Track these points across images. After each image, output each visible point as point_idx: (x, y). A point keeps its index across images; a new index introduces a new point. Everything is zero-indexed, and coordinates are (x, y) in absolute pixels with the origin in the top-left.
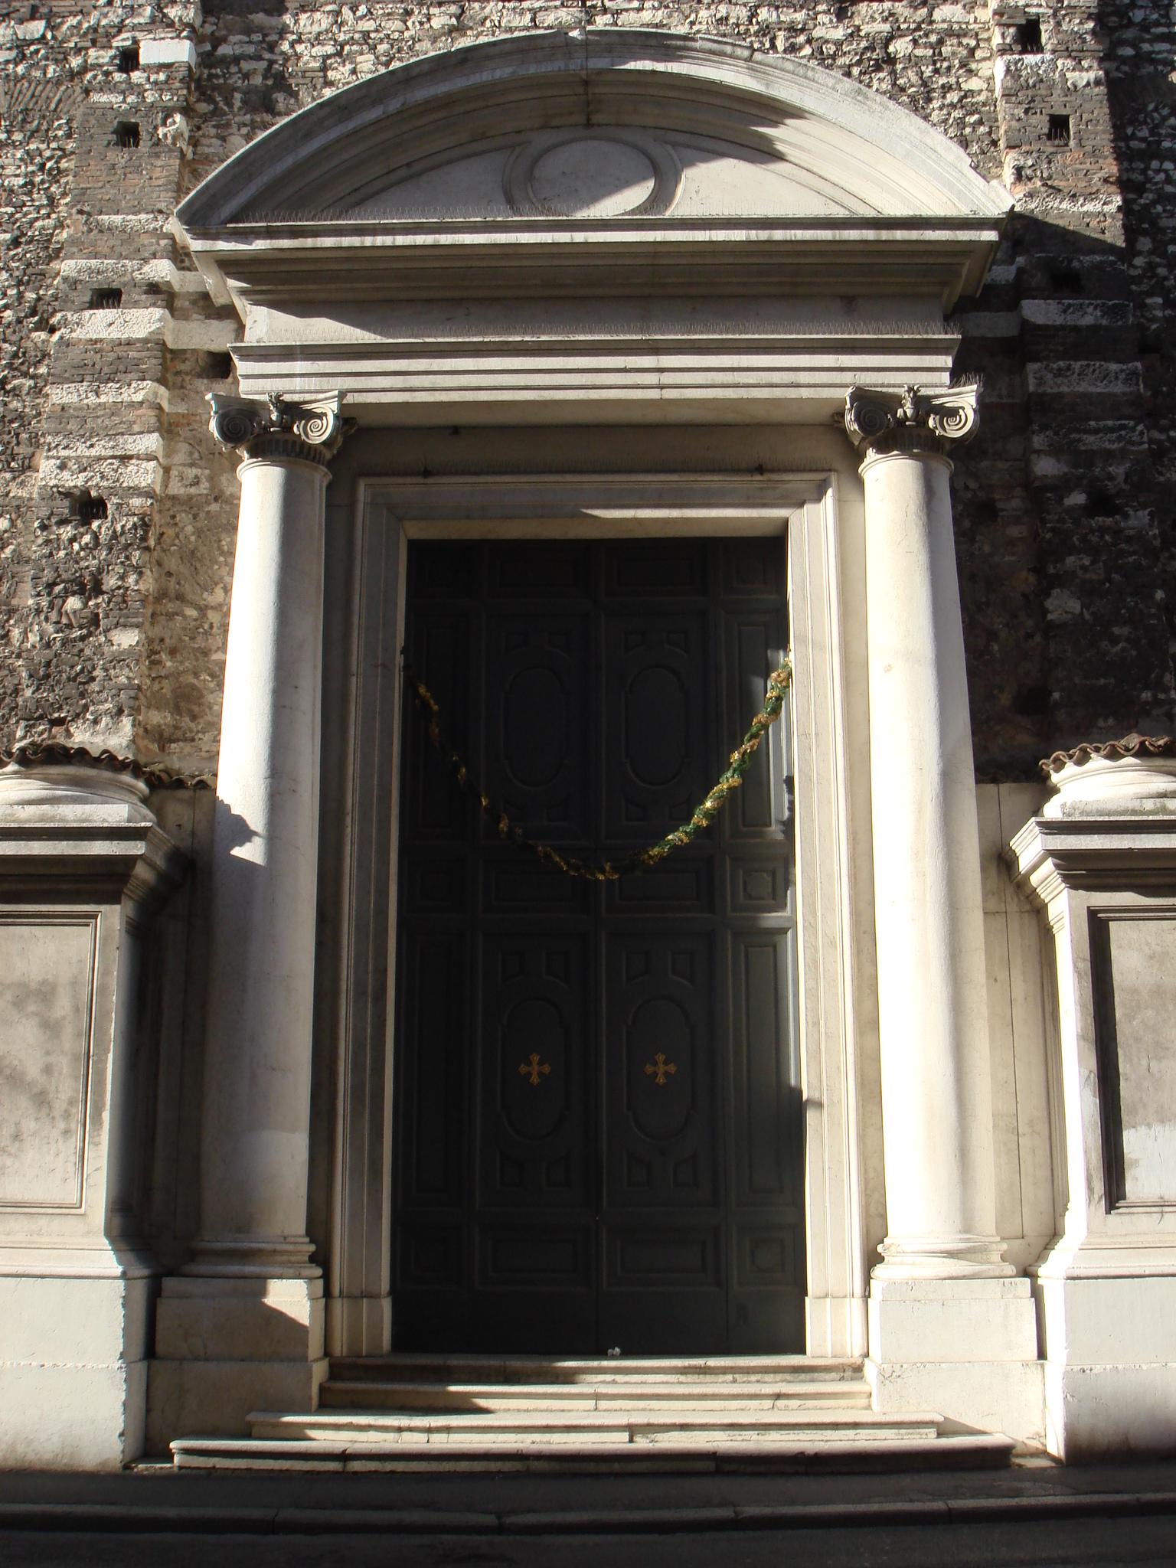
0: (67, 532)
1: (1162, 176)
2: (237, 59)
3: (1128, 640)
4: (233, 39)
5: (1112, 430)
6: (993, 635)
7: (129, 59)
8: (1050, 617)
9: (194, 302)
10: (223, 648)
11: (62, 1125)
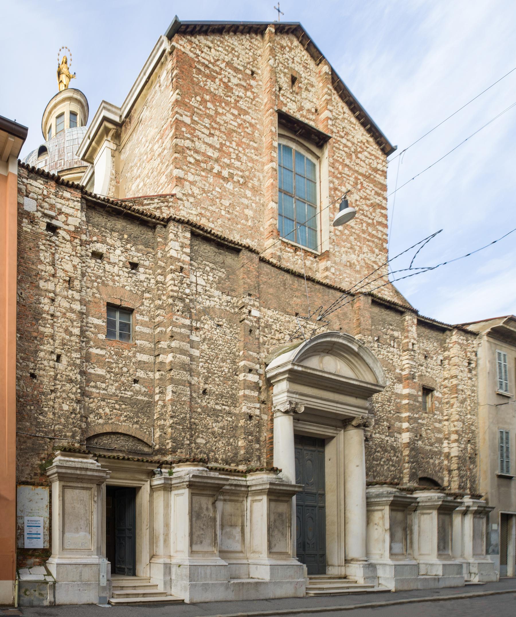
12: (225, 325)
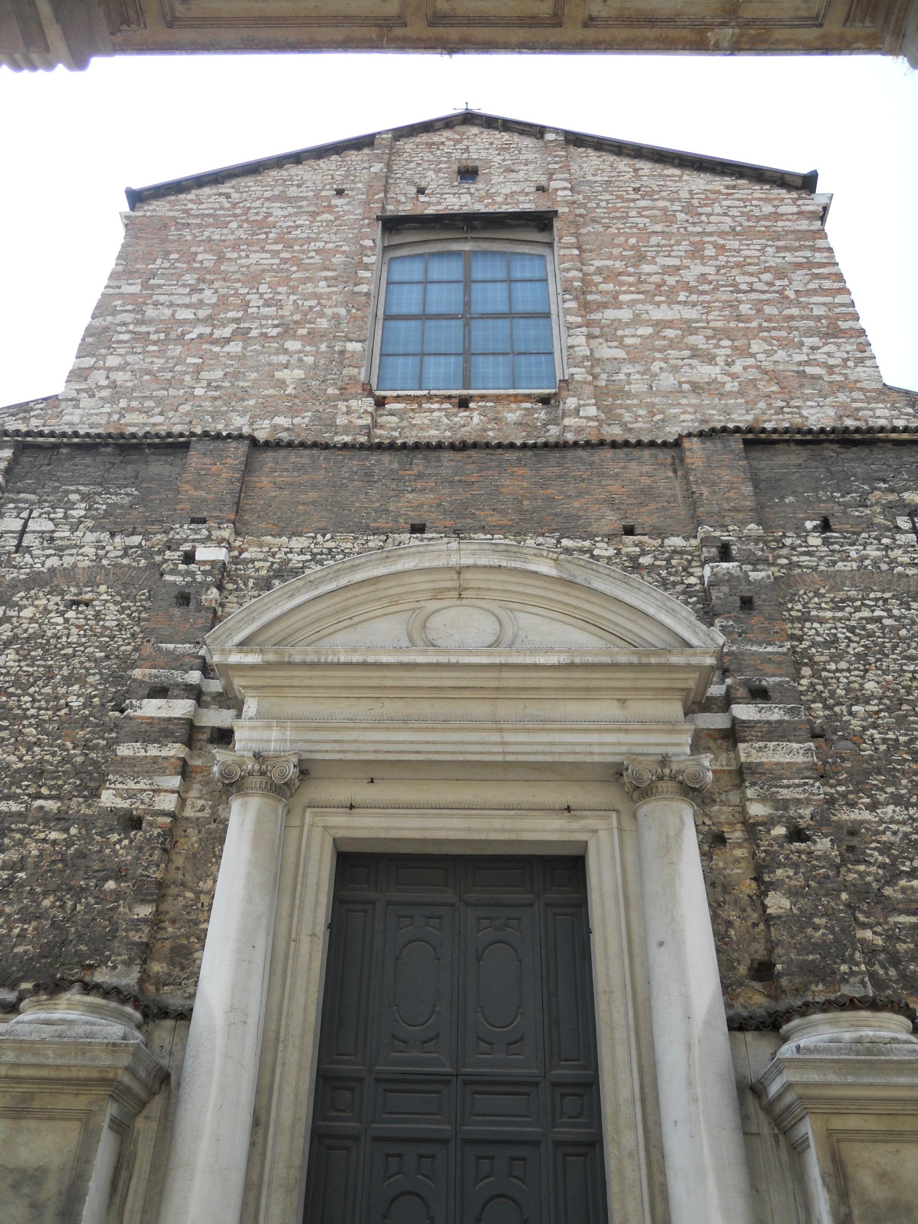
3: (826, 927)
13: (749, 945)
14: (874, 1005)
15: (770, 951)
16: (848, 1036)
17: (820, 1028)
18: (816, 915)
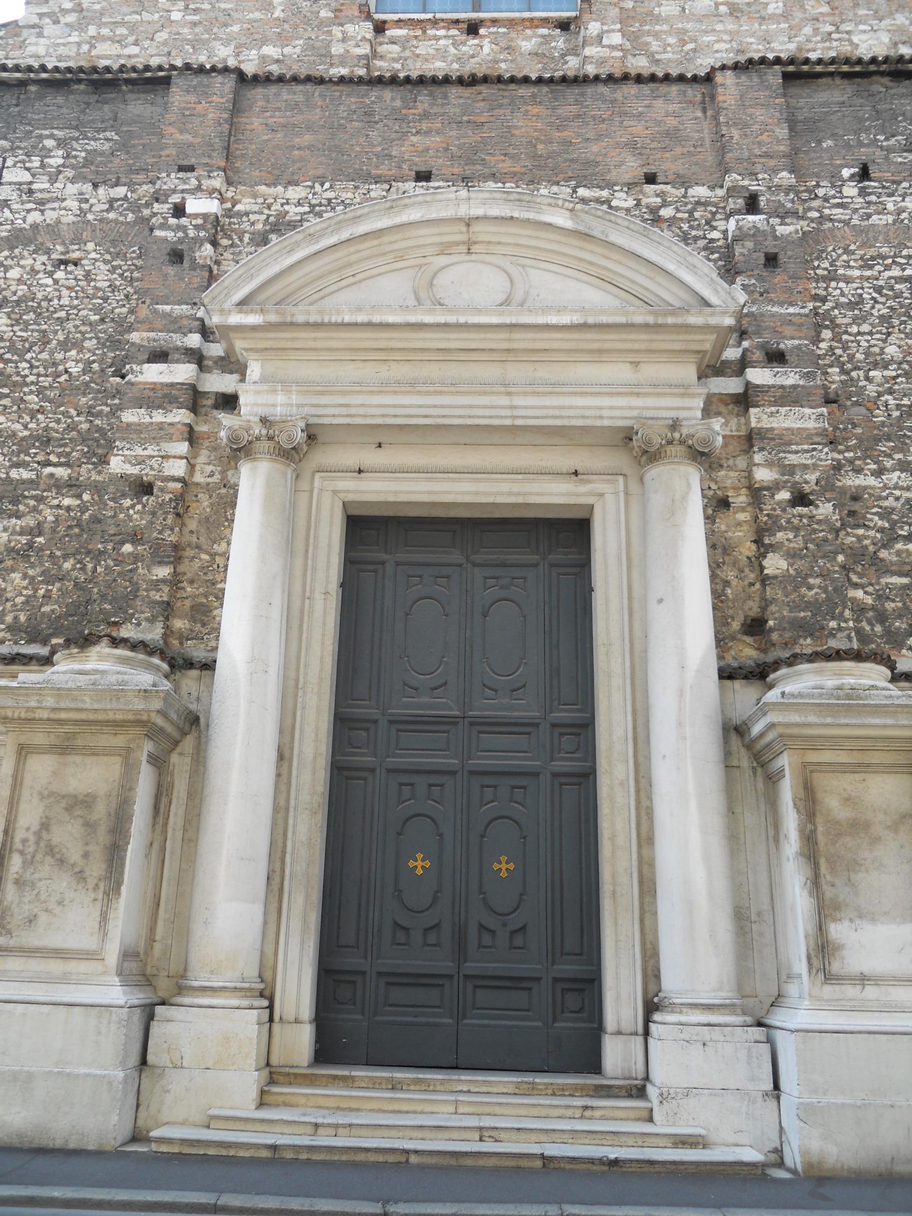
0: (127, 502)
1: (839, 291)
2: (247, 214)
3: (820, 587)
4: (245, 200)
5: (807, 451)
6: (727, 583)
7: (179, 211)
8: (766, 572)
9: (215, 363)
10: (224, 580)
11: (92, 895)
12: (93, 255)
13: (744, 602)
14: (858, 657)
15: (764, 609)
16: (830, 683)
17: (805, 676)
18: (811, 576)
